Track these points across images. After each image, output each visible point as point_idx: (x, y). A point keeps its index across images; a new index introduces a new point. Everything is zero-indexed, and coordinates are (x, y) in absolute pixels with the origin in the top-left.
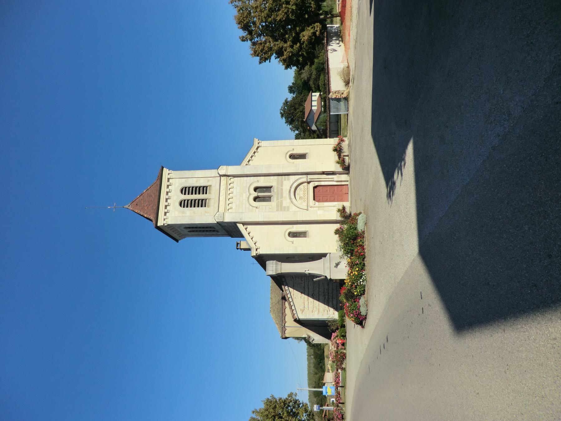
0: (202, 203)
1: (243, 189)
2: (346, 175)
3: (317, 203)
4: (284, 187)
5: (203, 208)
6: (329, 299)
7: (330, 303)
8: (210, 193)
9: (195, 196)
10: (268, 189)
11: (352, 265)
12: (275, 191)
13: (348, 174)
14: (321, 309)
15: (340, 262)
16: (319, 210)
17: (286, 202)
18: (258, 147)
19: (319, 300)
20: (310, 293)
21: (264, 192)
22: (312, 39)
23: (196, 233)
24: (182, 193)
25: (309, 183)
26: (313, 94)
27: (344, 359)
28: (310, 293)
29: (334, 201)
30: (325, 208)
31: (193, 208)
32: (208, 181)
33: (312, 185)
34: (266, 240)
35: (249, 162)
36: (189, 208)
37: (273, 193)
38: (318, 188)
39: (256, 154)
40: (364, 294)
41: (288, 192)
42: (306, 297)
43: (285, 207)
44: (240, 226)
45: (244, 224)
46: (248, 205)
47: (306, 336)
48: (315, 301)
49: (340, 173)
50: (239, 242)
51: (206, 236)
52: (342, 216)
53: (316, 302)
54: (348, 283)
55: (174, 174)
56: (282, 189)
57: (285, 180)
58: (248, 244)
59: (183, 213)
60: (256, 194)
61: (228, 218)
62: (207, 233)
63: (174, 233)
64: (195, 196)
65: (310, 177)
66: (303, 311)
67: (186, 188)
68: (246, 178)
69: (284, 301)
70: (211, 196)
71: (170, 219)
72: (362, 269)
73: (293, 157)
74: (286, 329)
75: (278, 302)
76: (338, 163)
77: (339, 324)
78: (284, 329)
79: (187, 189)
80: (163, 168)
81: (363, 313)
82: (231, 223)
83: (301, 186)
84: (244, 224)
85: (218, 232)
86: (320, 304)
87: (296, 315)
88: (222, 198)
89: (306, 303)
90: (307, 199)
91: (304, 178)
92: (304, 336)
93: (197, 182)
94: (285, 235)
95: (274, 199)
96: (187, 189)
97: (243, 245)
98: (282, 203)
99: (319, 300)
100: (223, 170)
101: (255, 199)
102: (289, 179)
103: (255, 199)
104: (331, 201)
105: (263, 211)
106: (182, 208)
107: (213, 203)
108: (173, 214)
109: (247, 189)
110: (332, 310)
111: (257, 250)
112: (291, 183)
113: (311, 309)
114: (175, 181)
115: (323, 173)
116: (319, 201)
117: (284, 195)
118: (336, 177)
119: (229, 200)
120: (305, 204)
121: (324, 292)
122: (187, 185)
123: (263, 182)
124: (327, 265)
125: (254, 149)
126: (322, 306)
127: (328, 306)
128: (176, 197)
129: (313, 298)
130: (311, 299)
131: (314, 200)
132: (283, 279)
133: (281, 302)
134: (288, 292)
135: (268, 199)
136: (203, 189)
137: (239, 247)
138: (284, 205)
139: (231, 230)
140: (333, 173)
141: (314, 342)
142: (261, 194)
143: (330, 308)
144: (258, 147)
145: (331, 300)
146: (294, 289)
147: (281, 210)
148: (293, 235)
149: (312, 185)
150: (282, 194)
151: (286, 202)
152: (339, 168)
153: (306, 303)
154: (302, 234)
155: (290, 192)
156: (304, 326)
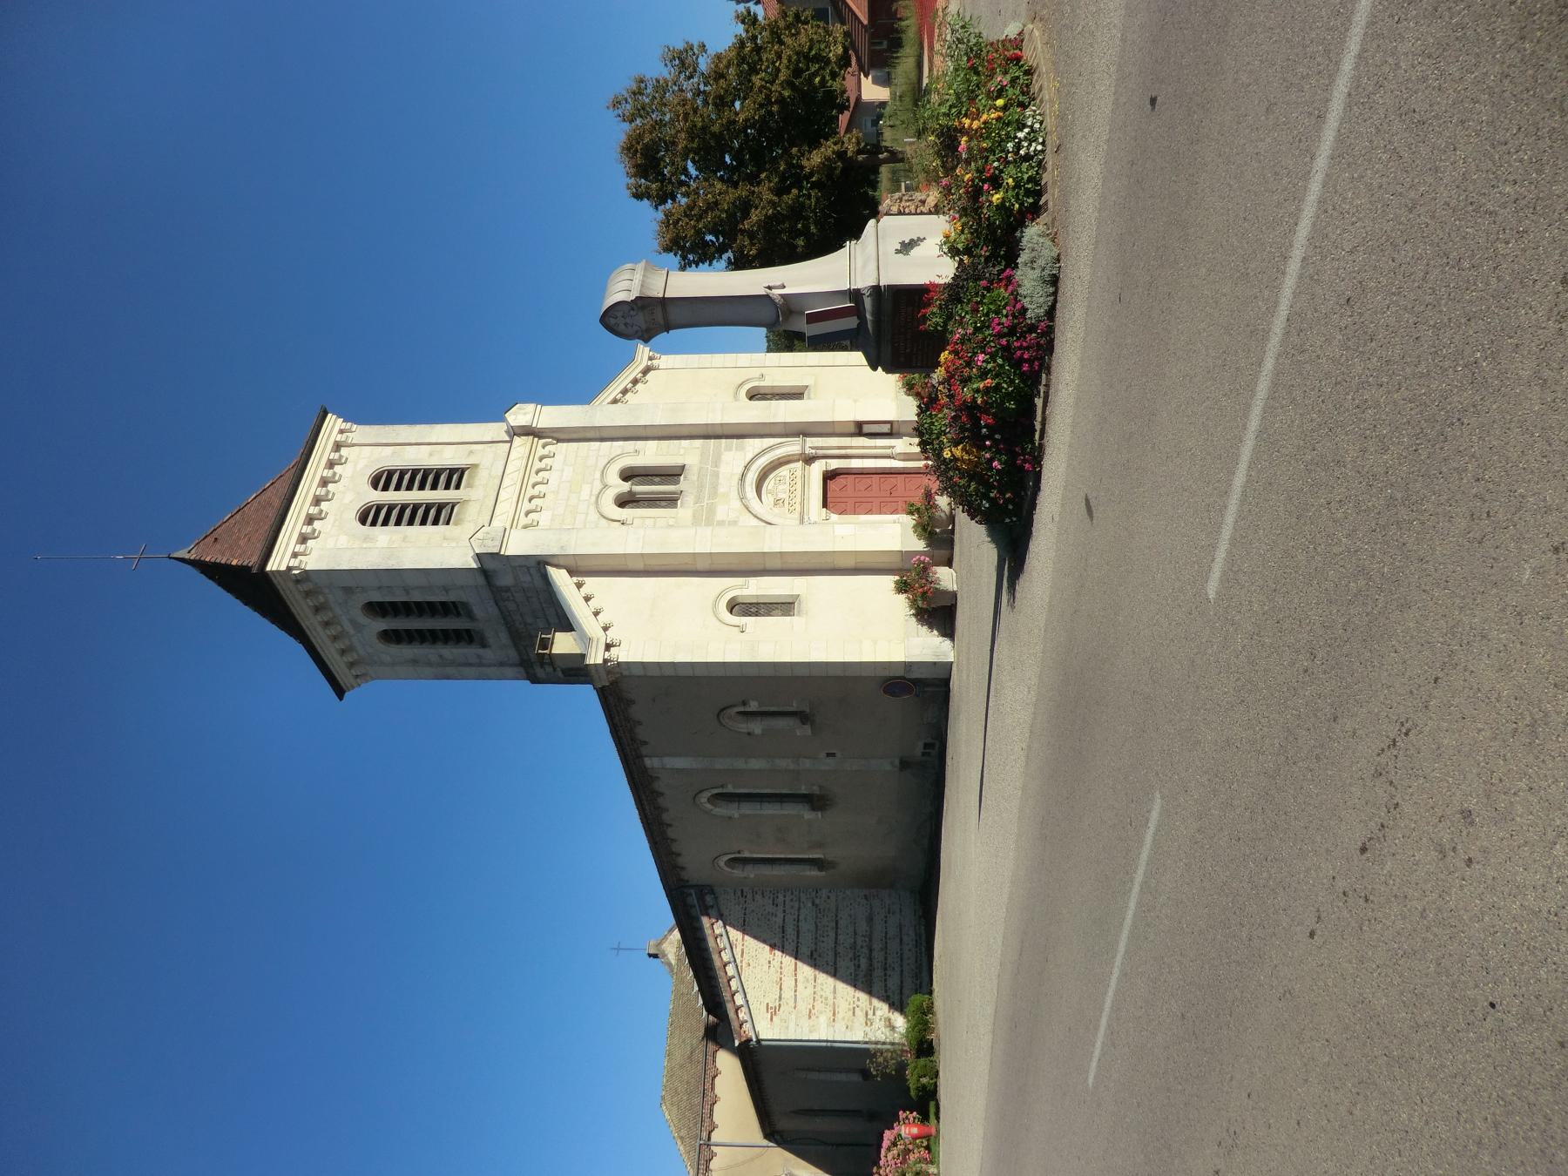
0: (437, 514)
3: (834, 517)
4: (724, 469)
5: (441, 528)
6: (871, 969)
10: (672, 474)
14: (843, 1008)
15: (920, 240)
18: (646, 371)
19: (835, 974)
20: (805, 950)
22: (832, 169)
25: (809, 460)
28: (805, 950)
33: (818, 468)
38: (840, 481)
39: (639, 386)
42: (788, 961)
44: (559, 577)
55: (360, 433)
56: (716, 475)
57: (729, 449)
60: (625, 487)
64: (415, 496)
65: (811, 442)
66: (773, 1011)
69: (712, 1047)
71: (314, 555)
73: (754, 395)
74: (713, 1155)
80: (325, 414)
83: (784, 471)
89: (788, 983)
91: (793, 446)
100: (521, 415)
102: (742, 448)
103: (624, 501)
105: (648, 533)
108: (329, 532)
109: (598, 475)
111: (608, 647)
113: (803, 1007)
119: (527, 491)
121: (854, 946)
123: (651, 454)
126: (847, 994)
128: (352, 490)
130: (806, 971)
131: (825, 505)
134: (723, 943)
143: (875, 1002)
146: (744, 932)
149: (818, 468)
150: (715, 487)
151: (728, 507)
153: (788, 983)
154: (785, 607)
155: (747, 467)
156: (779, 1144)
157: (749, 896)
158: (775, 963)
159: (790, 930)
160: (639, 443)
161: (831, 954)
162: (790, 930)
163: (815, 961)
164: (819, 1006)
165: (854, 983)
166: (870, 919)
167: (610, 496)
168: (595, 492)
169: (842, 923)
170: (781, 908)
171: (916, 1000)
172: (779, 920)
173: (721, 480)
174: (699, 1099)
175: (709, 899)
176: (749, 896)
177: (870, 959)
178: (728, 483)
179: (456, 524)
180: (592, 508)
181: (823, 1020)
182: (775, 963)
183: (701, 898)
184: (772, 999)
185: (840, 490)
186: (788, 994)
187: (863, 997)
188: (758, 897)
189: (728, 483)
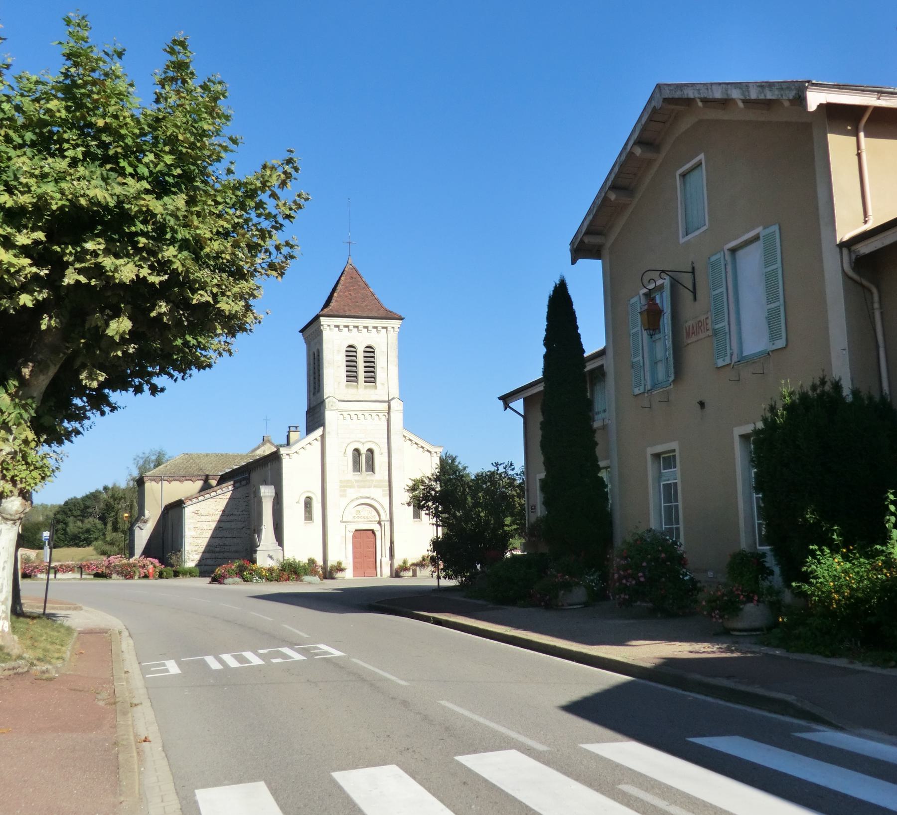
0: (352, 376)
1: (370, 434)
2: (389, 574)
7: (208, 555)
8: (366, 387)
9: (362, 366)
10: (371, 467)
11: (271, 570)
12: (368, 478)
13: (392, 576)
17: (352, 493)
19: (212, 537)
20: (222, 524)
21: (367, 462)
23: (312, 363)
24: (367, 347)
25: (379, 523)
27: (126, 576)
28: (222, 524)
29: (354, 557)
31: (345, 364)
32: (383, 384)
33: (376, 527)
34: (299, 472)
35: (410, 440)
36: (345, 358)
37: (365, 475)
40: (245, 581)
42: (217, 518)
43: (345, 491)
44: (319, 432)
45: (323, 437)
47: (147, 517)
48: (211, 532)
49: (392, 566)
50: (299, 429)
51: (309, 364)
52: (332, 567)
53: (209, 534)
54: (254, 567)
55: (393, 336)
56: (369, 487)
57: (383, 491)
58: (297, 442)
59: (339, 351)
60: (363, 451)
61: (330, 416)
62: (312, 378)
63: (311, 332)
64: (362, 366)
65: (388, 525)
66: (196, 513)
67: (373, 352)
68: (386, 436)
70: (362, 390)
72: (267, 579)
74: (157, 482)
75: (201, 469)
76: (405, 562)
77: (178, 568)
78: (158, 479)
79: (372, 354)
81: (226, 581)
82: (324, 419)
84: (323, 437)
85: (314, 394)
86: (207, 540)
87: (190, 502)
89: (209, 518)
91: (385, 516)
92: (146, 512)
95: (357, 476)
96: (372, 354)
97: (294, 436)
98: (351, 487)
99: (213, 537)
100: (396, 405)
101: (357, 451)
103: (357, 451)
104: (354, 552)
106: (345, 349)
107: (352, 392)
108: (337, 336)
110: (197, 557)
113: (199, 525)
114: (382, 337)
115: (392, 543)
116: (354, 537)
117: (362, 490)
118: (386, 560)
119: (353, 417)
120: (350, 519)
121: (225, 545)
122: (378, 355)
123: (380, 460)
124: (271, 547)
125: (427, 446)
126: (203, 542)
127: (204, 552)
128: (361, 340)
129: (216, 529)
130: (213, 525)
133: (201, 473)
135: (357, 466)
136: (371, 378)
137: (292, 429)
139: (315, 417)
140: (392, 556)
141: (137, 531)
145: (214, 555)
146: (230, 499)
147: (341, 486)
148: (308, 503)
150: (364, 487)
151: (352, 493)
152: (398, 563)
153: (209, 518)
156: (163, 512)
158: (217, 512)
159: (232, 518)
160: (387, 454)
162: (232, 518)
163: (218, 529)
164: (199, 531)
165: (208, 545)
166: (236, 552)
171: (198, 570)
172: (236, 513)
174: (182, 474)
175: (244, 483)
178: (365, 492)
179: (347, 386)
181: (193, 533)
182: (217, 512)
183: (244, 479)
184: (202, 512)
185: (364, 540)
186: (204, 518)
187: (202, 549)
189: (365, 492)
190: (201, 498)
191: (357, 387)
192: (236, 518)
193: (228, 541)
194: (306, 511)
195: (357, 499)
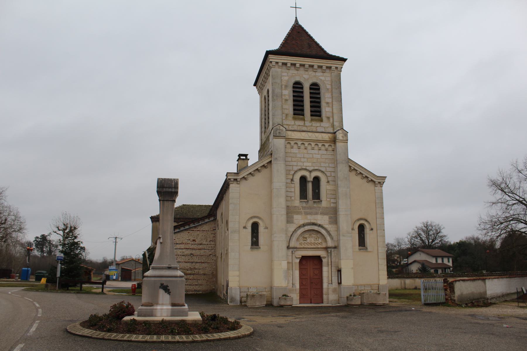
3: (298, 261)
16: (288, 263)
23: (263, 107)
26: (451, 260)
30: (291, 272)
41: (313, 221)
46: (295, 168)
56: (316, 214)
60: (310, 178)
62: (263, 120)
67: (319, 89)
88: (304, 136)
90: (304, 248)
93: (327, 103)
94: (255, 217)
103: (303, 179)
104: (301, 278)
106: (292, 85)
109: (316, 168)
112: (326, 226)
117: (309, 217)
121: (195, 269)
122: (322, 91)
128: (307, 78)
132: (212, 219)
138: (296, 217)
142: (310, 186)
144: (374, 182)
150: (311, 214)
151: (299, 220)
157: (213, 232)
161: (192, 261)
162: (201, 247)
167: (306, 174)
168: (308, 168)
169: (203, 264)
170: (209, 243)
172: (204, 243)
173: (313, 216)
176: (213, 232)
177: (190, 274)
180: (300, 167)
186: (178, 246)
188: (213, 235)
189: (311, 219)
190: (516, 304)
191: (304, 120)
192: (205, 247)
193: (197, 266)
194: (253, 237)
195: (304, 225)
